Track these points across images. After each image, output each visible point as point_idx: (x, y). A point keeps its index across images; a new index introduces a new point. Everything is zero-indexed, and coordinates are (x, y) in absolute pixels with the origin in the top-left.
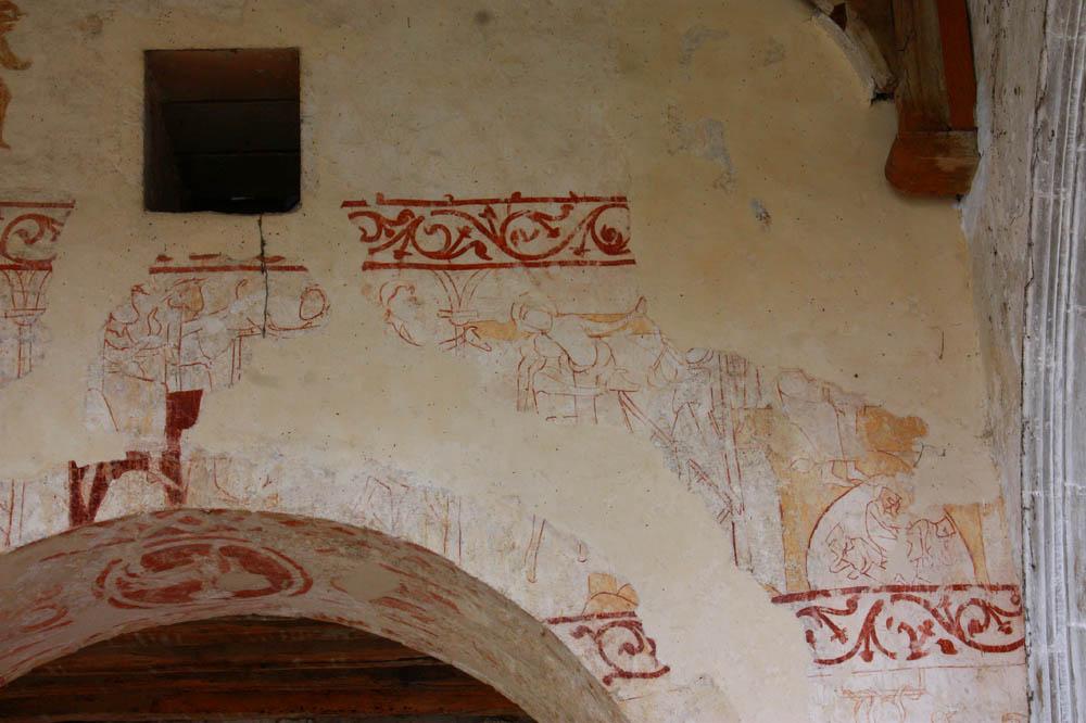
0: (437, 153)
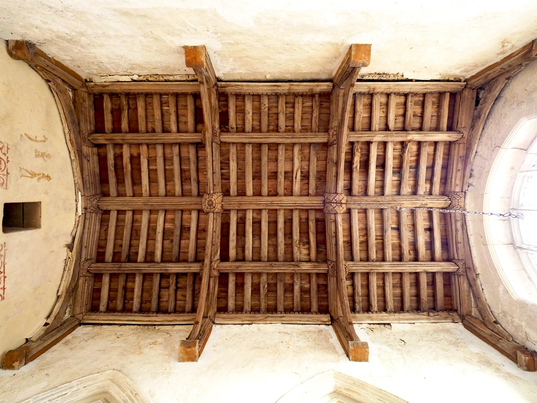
0: (17, 259)
